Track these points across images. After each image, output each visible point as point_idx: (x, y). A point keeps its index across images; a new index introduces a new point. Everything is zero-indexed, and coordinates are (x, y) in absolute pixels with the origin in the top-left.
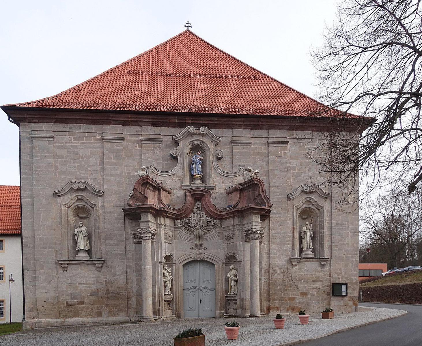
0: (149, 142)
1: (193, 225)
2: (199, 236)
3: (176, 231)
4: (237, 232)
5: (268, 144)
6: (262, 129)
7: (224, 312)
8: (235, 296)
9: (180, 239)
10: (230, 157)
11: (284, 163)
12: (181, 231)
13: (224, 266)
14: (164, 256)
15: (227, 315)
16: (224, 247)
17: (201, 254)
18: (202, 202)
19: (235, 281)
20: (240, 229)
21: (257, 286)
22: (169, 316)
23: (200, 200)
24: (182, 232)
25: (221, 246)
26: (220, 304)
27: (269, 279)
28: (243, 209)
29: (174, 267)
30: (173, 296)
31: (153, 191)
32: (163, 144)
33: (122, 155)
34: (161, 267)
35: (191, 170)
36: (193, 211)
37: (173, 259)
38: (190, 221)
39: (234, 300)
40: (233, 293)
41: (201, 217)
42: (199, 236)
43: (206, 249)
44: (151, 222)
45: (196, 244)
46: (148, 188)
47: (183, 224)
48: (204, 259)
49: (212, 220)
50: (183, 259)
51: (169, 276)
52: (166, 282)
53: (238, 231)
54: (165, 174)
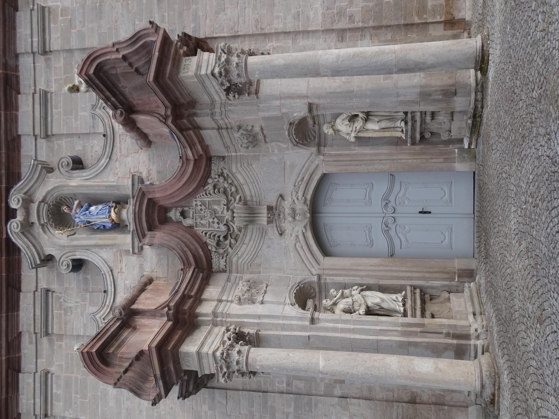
0: (50, 317)
1: (223, 228)
2: (247, 215)
3: (239, 269)
4: (234, 119)
5: (45, 52)
6: (16, 68)
7: (459, 149)
8: (413, 118)
9: (258, 261)
10: (75, 139)
11: (84, 13)
12: (239, 258)
13: (326, 150)
14: (296, 311)
15: (471, 138)
16: (276, 151)
17: (293, 210)
18: (170, 206)
19: (366, 120)
20: (223, 109)
21: (383, 52)
22: (469, 304)
23: (165, 210)
24: (241, 256)
25: (275, 158)
26: (434, 160)
27: (362, 29)
28: (168, 104)
29: (329, 280)
30: (409, 288)
31: (135, 329)
32: (54, 286)
33: (77, 378)
34: (327, 321)
35: (103, 229)
36: (191, 227)
37: (307, 280)
38: (214, 235)
39: (423, 122)
40: (403, 124)
41: (203, 207)
42: (247, 215)
43: (281, 196)
44: (203, 344)
45: (269, 222)
46: (119, 346)
47: (221, 251)
48: (308, 202)
49: (210, 181)
50: (309, 256)
51: (352, 296)
52: (368, 307)
53: (231, 116)
54: (111, 289)
